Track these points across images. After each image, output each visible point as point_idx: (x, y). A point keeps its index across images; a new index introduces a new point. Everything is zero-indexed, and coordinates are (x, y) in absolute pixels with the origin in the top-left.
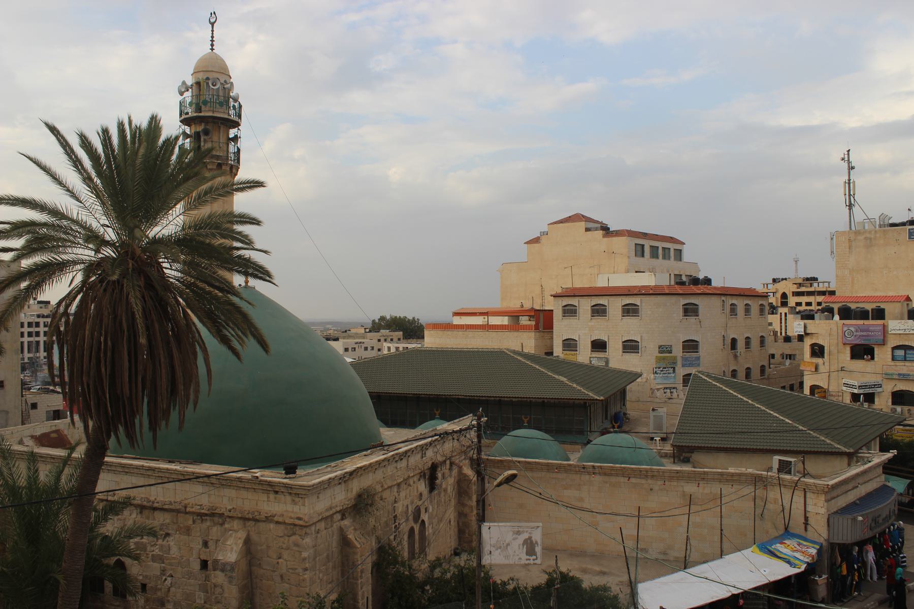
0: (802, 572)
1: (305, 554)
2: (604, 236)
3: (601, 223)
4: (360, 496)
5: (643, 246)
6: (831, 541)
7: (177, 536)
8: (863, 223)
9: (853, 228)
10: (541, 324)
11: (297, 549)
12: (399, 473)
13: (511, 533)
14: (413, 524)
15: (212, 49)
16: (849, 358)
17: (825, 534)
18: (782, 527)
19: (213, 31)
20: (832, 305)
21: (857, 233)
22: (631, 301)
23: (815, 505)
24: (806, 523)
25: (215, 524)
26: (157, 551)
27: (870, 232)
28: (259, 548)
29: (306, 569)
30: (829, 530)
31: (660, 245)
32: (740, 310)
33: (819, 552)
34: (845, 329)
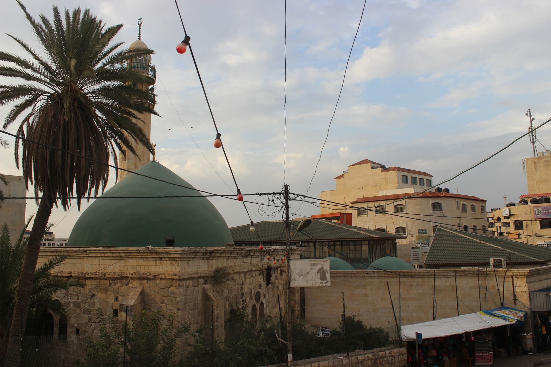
0: (513, 324)
1: (178, 299)
2: (383, 171)
3: (381, 165)
4: (217, 271)
5: (407, 177)
6: (533, 310)
7: (99, 295)
8: (543, 153)
9: (536, 156)
10: (345, 222)
11: (173, 296)
12: (245, 265)
13: (310, 265)
14: (255, 303)
15: (139, 39)
16: (539, 228)
17: (529, 306)
18: (500, 304)
19: (140, 29)
20: (526, 199)
21: (539, 158)
22: (399, 203)
23: (520, 286)
24: (515, 299)
25: (123, 285)
26: (87, 307)
27: (547, 157)
28: (150, 298)
29: (179, 309)
30: (530, 302)
31: (418, 176)
32: (469, 208)
33: (526, 315)
34: (535, 209)
